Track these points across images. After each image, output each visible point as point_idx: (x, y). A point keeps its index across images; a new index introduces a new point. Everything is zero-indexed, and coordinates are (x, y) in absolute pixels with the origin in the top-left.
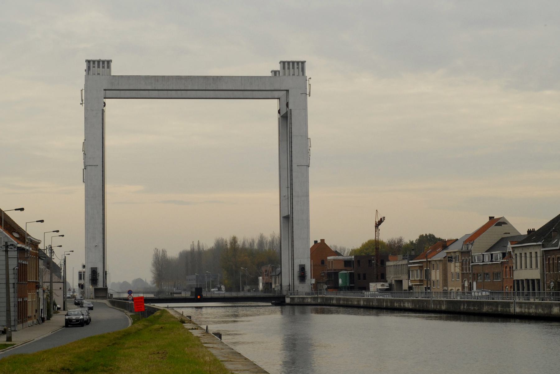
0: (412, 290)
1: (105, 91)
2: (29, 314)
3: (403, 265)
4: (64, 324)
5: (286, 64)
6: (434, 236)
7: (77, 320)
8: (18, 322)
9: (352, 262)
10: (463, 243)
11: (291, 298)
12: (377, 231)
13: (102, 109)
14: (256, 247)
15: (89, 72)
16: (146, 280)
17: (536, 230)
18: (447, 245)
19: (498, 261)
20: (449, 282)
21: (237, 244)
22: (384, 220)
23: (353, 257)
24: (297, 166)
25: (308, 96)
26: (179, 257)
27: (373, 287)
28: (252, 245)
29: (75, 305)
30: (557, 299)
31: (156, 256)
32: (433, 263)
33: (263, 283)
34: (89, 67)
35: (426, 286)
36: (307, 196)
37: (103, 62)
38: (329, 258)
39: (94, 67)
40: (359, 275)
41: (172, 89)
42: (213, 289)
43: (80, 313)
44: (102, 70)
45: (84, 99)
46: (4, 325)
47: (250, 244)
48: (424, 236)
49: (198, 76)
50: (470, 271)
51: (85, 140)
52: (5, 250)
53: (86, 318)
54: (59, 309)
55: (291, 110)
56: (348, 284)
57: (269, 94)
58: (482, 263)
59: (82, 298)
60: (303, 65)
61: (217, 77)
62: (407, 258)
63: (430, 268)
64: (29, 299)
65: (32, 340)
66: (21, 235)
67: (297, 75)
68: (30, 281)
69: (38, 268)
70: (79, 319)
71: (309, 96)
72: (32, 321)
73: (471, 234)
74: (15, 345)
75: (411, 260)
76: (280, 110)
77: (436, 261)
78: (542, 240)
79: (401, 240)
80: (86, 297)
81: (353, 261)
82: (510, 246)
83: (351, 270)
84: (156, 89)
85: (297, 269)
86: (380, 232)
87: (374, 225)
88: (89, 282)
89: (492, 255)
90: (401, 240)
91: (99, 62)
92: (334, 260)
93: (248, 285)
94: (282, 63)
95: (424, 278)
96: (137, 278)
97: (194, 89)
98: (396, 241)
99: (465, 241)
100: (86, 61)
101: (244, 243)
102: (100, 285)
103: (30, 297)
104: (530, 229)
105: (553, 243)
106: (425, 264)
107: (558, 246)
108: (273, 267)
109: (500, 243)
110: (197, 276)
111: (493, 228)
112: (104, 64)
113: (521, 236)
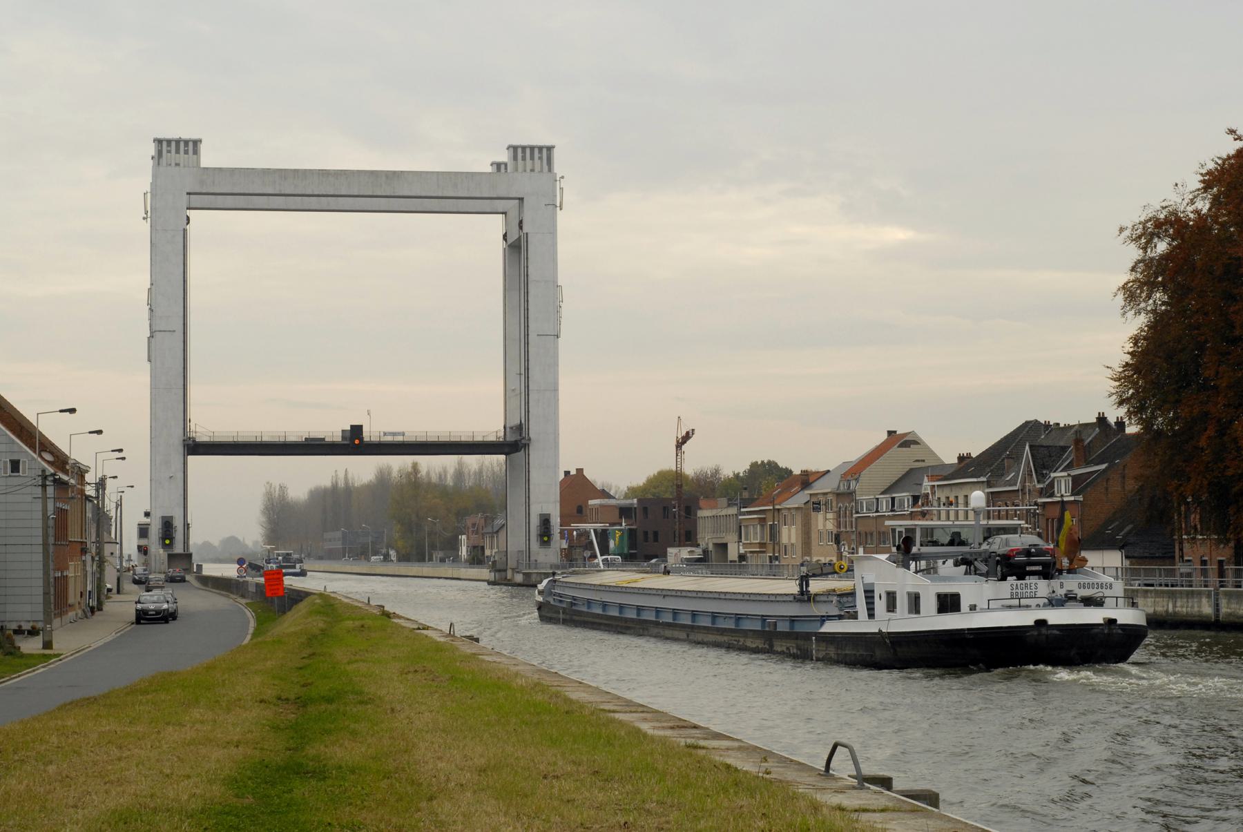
0: (744, 561)
1: (188, 196)
2: (71, 600)
3: (729, 515)
4: (134, 619)
5: (520, 150)
6: (776, 464)
7: (158, 612)
8: (55, 614)
9: (633, 509)
10: (839, 477)
11: (524, 574)
12: (679, 454)
13: (184, 229)
14: (450, 481)
15: (161, 160)
16: (244, 539)
17: (974, 455)
18: (810, 481)
19: (905, 511)
20: (813, 548)
21: (419, 476)
22: (694, 436)
23: (635, 501)
24: (538, 335)
25: (558, 208)
26: (308, 499)
27: (674, 555)
28: (443, 477)
29: (133, 585)
30: (1184, 583)
31: (269, 496)
32: (785, 512)
33: (468, 546)
34: (160, 153)
35: (771, 555)
36: (555, 390)
37: (186, 142)
38: (591, 502)
39: (169, 152)
40: (646, 533)
41: (311, 193)
42: (375, 557)
43: (162, 598)
44: (167, 156)
45: (149, 209)
46: (29, 619)
47: (440, 475)
48: (760, 465)
49: (305, 171)
50: (852, 527)
51: (152, 284)
52: (40, 484)
53: (172, 608)
54: (109, 590)
55: (527, 234)
56: (626, 551)
57: (486, 205)
58: (874, 514)
59: (147, 572)
60: (550, 154)
61: (394, 172)
62: (737, 504)
63: (779, 521)
64: (70, 573)
65: (87, 648)
66: (57, 457)
67: (539, 170)
68: (73, 540)
69: (84, 516)
70: (161, 610)
71: (561, 209)
72: (74, 613)
73: (855, 461)
74: (62, 657)
75: (743, 507)
76: (506, 233)
77: (789, 509)
78: (987, 474)
79: (717, 471)
80: (153, 569)
81: (635, 508)
82: (927, 484)
83: (632, 525)
84: (283, 192)
85: (535, 522)
86: (686, 456)
87: (675, 443)
88: (158, 543)
89: (893, 499)
90: (717, 471)
91: (178, 142)
92: (602, 506)
93: (440, 550)
94: (511, 150)
95: (767, 540)
96: (228, 535)
97: (351, 194)
98: (709, 472)
99: (844, 474)
100: (154, 141)
101: (428, 473)
102: (178, 549)
103: (71, 569)
104: (963, 454)
105: (1008, 479)
106: (769, 516)
107: (1016, 485)
108: (486, 519)
109: (909, 477)
110: (343, 532)
111: (895, 451)
112: (188, 147)
113: (944, 466)
